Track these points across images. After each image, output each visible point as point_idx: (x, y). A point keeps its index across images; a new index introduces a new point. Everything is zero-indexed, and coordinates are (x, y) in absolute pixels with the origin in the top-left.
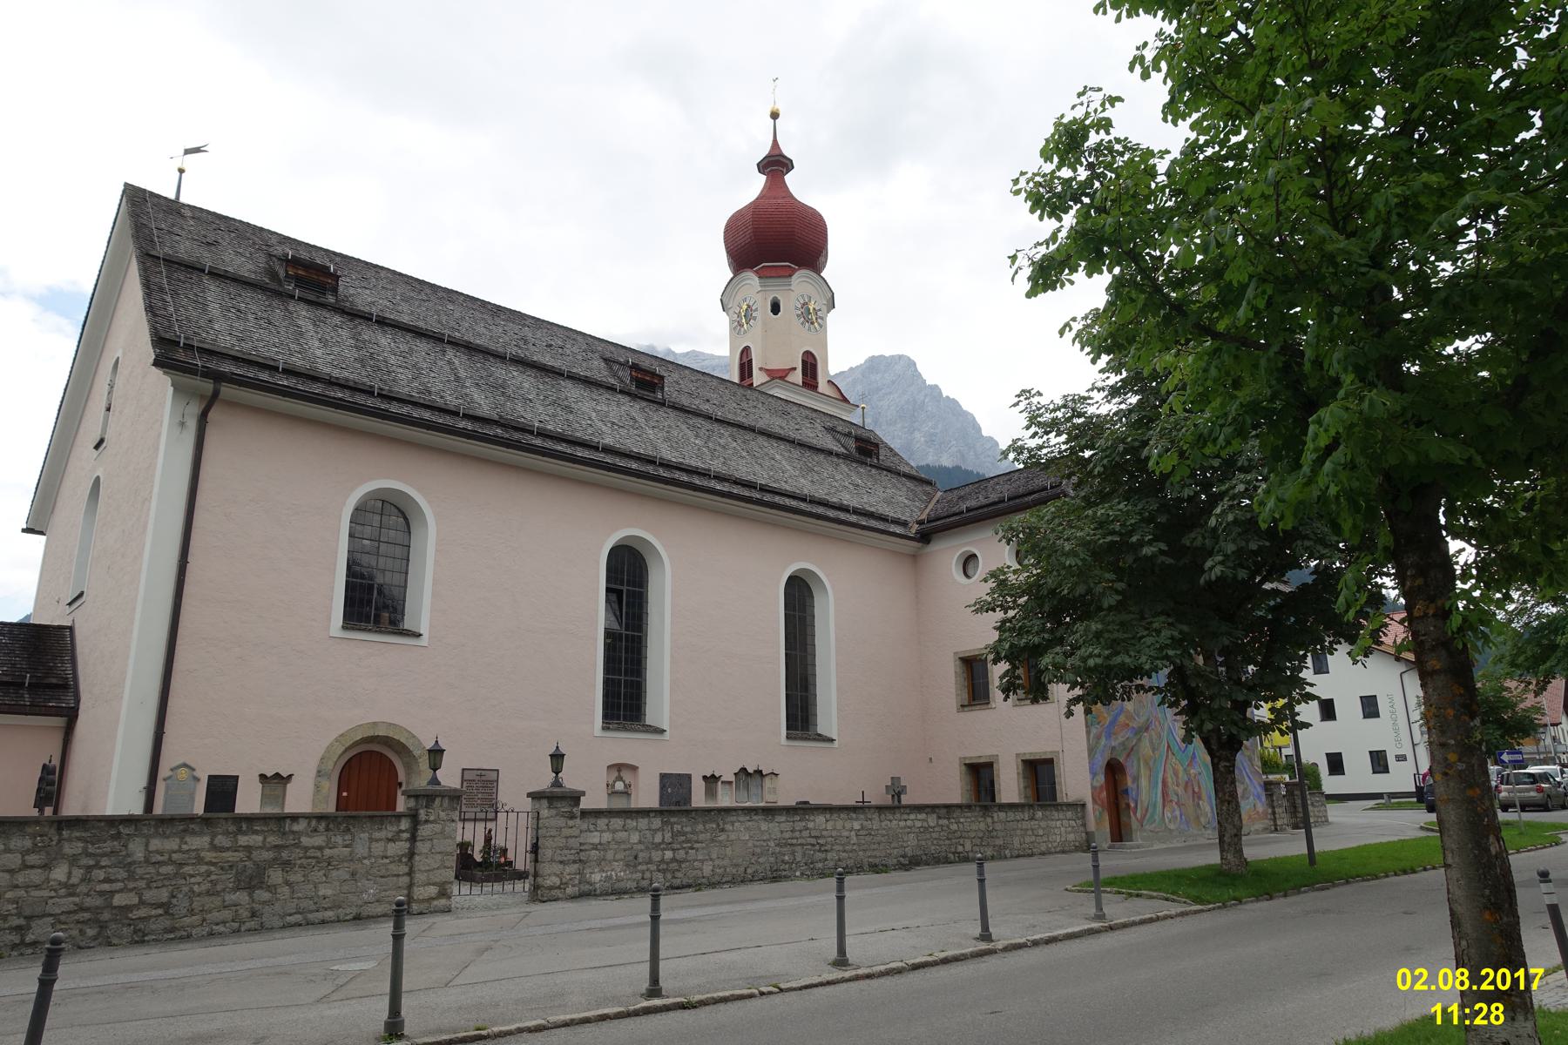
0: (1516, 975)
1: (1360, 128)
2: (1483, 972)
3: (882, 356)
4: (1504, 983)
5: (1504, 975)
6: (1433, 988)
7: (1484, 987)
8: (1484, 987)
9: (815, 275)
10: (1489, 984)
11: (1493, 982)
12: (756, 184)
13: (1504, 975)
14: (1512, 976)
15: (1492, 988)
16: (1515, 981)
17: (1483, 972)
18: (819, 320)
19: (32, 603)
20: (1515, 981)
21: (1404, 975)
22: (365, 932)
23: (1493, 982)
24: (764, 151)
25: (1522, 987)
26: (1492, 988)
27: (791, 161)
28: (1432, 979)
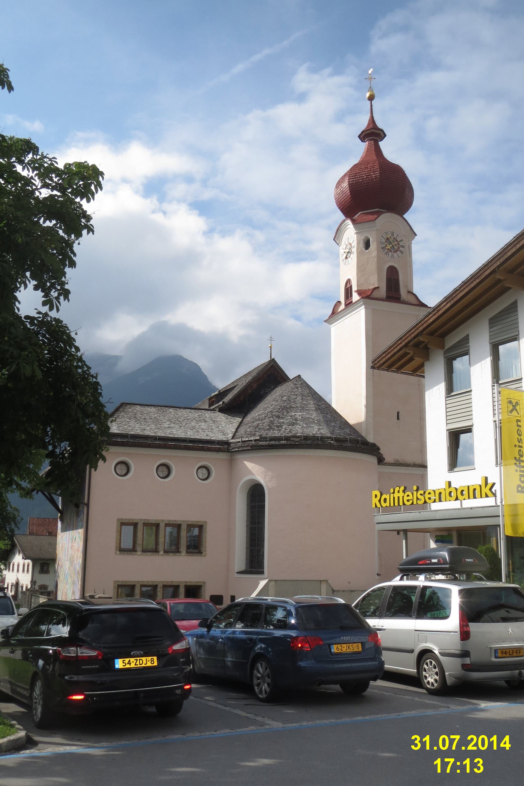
0: (491, 740)
1: (93, 185)
2: (469, 738)
3: (17, 298)
4: (483, 745)
5: (483, 740)
6: (435, 748)
7: (470, 748)
8: (470, 748)
9: (399, 217)
10: (473, 746)
11: (476, 745)
12: (362, 147)
13: (483, 740)
14: (489, 740)
15: (475, 748)
16: (491, 744)
17: (469, 738)
18: (401, 249)
19: (363, 410)
20: (491, 744)
21: (444, 740)
22: (511, 704)
23: (476, 745)
24: (363, 123)
25: (428, 748)
26: (475, 748)
27: (383, 131)
28: (434, 742)
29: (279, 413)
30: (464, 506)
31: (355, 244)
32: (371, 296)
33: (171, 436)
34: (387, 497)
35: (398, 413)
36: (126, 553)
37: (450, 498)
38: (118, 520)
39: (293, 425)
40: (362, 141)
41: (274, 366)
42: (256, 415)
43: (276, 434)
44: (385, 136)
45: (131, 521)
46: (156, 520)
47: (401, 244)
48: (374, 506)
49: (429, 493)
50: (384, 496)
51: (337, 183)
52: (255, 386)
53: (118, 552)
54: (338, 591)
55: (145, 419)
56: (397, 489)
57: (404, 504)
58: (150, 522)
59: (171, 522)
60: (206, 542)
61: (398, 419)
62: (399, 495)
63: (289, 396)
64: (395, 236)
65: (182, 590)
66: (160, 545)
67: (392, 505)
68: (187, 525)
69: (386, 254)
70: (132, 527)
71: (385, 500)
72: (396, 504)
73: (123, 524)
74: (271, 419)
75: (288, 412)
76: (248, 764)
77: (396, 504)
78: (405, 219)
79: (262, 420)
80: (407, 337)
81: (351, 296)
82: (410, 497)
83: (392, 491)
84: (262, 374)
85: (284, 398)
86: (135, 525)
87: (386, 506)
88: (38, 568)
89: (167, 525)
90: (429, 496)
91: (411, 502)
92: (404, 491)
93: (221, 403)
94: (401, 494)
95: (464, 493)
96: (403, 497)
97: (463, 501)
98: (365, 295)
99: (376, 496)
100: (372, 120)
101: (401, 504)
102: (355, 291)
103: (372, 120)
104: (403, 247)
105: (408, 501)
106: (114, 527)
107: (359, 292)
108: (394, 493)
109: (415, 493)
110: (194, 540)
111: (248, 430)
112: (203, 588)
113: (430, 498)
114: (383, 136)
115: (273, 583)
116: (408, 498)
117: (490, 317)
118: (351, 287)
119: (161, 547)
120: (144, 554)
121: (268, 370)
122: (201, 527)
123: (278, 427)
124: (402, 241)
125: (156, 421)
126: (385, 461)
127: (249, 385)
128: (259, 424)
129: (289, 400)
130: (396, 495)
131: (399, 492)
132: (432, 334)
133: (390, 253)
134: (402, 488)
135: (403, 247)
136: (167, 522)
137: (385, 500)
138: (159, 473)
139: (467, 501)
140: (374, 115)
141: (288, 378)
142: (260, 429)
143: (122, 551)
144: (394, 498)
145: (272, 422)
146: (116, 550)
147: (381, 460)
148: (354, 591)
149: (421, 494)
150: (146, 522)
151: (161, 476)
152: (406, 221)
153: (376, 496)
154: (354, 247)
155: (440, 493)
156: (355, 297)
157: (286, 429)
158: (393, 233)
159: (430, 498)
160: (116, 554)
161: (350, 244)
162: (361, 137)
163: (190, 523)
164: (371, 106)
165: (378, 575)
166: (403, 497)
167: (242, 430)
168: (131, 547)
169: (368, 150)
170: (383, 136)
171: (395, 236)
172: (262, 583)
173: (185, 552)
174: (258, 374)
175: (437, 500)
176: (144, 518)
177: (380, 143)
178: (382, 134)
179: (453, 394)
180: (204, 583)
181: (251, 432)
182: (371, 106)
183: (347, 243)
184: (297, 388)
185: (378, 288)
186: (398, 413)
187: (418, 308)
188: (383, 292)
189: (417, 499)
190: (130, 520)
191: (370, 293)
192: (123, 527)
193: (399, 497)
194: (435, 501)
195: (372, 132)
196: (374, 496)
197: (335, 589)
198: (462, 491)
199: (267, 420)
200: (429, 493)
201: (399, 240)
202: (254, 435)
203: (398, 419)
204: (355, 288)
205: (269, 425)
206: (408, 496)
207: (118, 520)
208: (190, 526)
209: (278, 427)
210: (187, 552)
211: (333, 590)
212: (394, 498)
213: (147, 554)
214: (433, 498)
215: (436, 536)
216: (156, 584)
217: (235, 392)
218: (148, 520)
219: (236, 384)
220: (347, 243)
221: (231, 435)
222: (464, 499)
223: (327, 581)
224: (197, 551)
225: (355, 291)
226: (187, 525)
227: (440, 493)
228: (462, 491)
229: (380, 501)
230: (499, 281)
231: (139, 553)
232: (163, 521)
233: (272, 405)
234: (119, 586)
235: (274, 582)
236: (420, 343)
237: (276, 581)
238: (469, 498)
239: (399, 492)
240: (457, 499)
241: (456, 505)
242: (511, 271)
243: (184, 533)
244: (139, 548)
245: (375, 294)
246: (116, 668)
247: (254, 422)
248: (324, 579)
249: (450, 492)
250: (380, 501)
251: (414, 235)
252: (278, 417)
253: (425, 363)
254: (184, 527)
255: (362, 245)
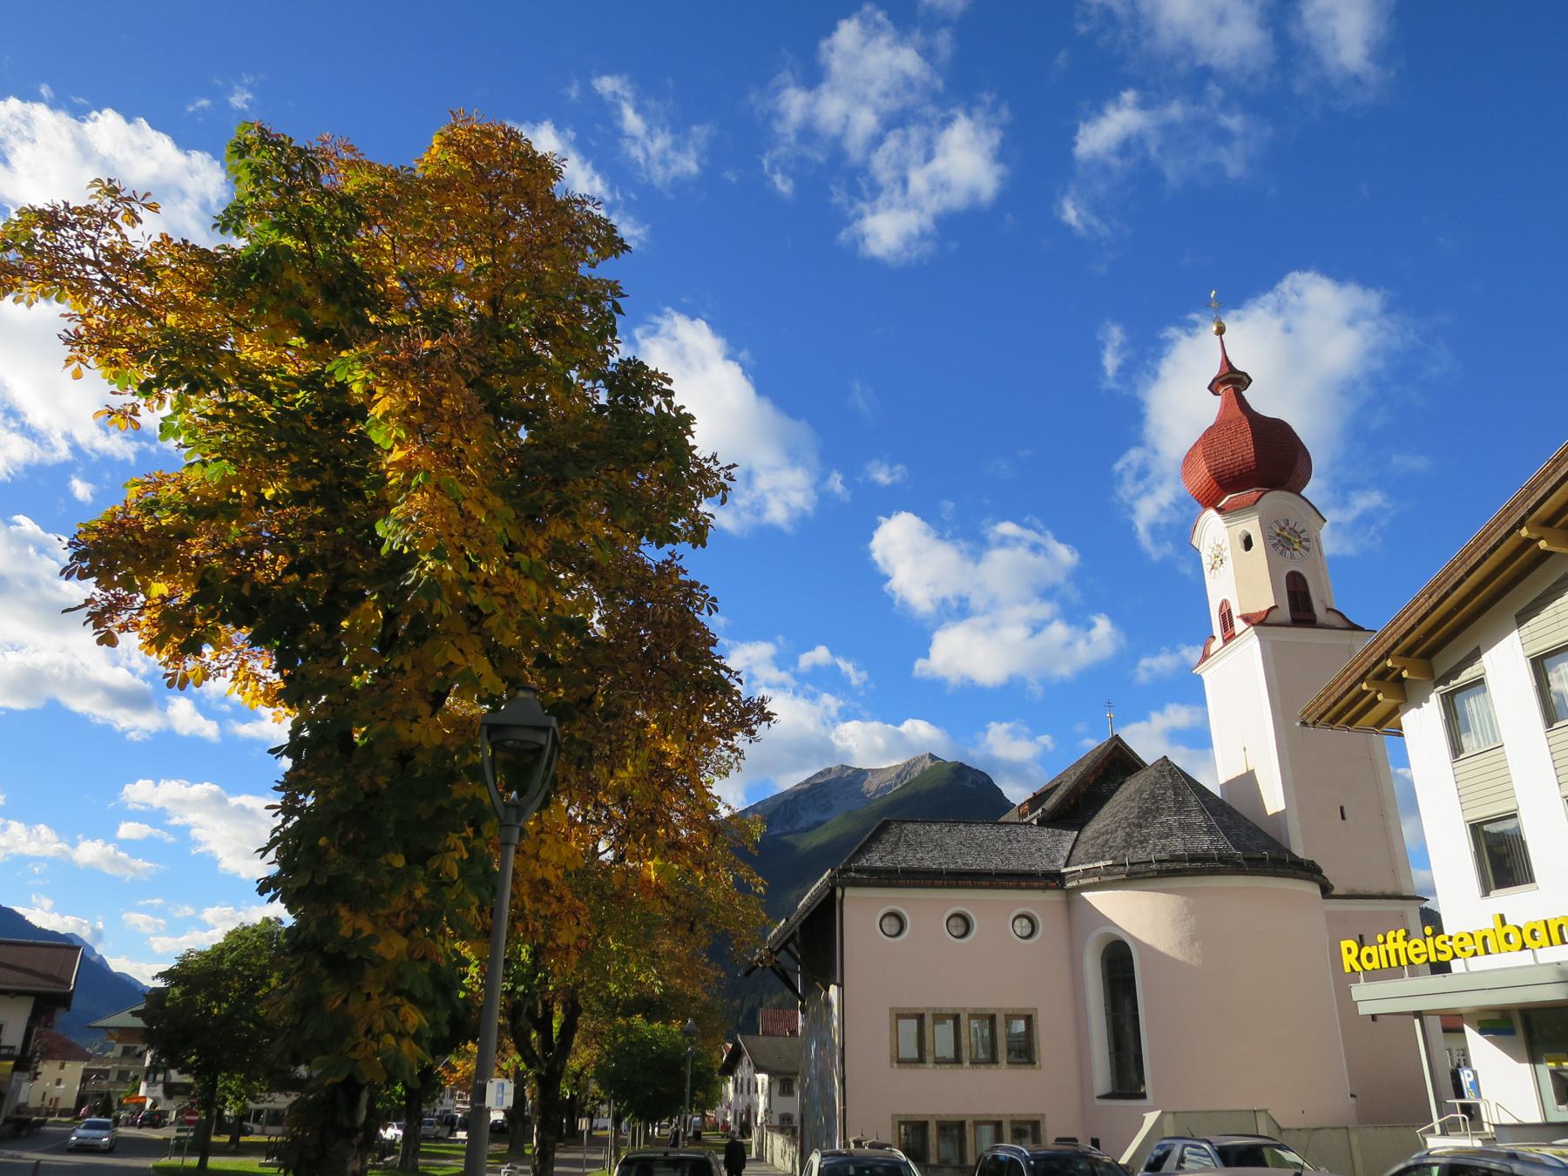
24: (1214, 370)
27: (1246, 374)
29: (1140, 818)
30: (1541, 961)
31: (1227, 545)
32: (1266, 621)
33: (967, 867)
34: (1373, 950)
35: (1342, 808)
36: (909, 1065)
37: (1538, 943)
38: (892, 1009)
39: (1167, 837)
40: (1215, 394)
41: (1120, 749)
42: (1101, 826)
43: (1141, 855)
44: (1250, 381)
45: (913, 1012)
46: (954, 1009)
47: (1303, 536)
48: (1348, 970)
49: (1461, 939)
50: (1365, 951)
51: (1195, 441)
52: (1091, 780)
53: (895, 1065)
54: (1289, 1130)
55: (921, 843)
56: (1391, 935)
57: (1410, 963)
58: (943, 1012)
59: (978, 1012)
60: (1039, 1044)
61: (1343, 818)
62: (1395, 946)
63: (1152, 792)
64: (1291, 525)
65: (1007, 1131)
66: (963, 1051)
67: (1385, 965)
68: (1006, 1015)
69: (1281, 553)
70: (915, 1021)
71: (1369, 957)
72: (1394, 963)
73: (900, 1016)
74: (1127, 830)
75: (1155, 818)
76: (772, 934)
77: (1394, 963)
78: (1303, 498)
79: (1111, 833)
80: (1361, 665)
81: (1232, 625)
82: (1422, 949)
83: (1380, 938)
84: (1101, 760)
85: (1145, 796)
86: (920, 1018)
87: (1374, 969)
88: (777, 1088)
89: (972, 1016)
90: (1461, 944)
91: (1423, 958)
92: (1406, 938)
93: (1040, 811)
94: (1401, 944)
95: (1537, 934)
96: (1406, 949)
97: (1537, 951)
98: (1255, 621)
99: (1349, 951)
100: (1226, 361)
101: (1404, 962)
102: (1238, 617)
103: (1226, 361)
104: (1307, 540)
105: (1417, 956)
106: (885, 1020)
107: (1246, 618)
108: (1385, 942)
109: (1429, 940)
110: (1019, 1041)
111: (1091, 851)
112: (1042, 1125)
113: (1463, 949)
114: (1247, 381)
115: (1169, 1118)
116: (1417, 951)
117: (1517, 611)
118: (1229, 611)
119: (965, 1054)
120: (938, 1067)
121: (1110, 754)
122: (1029, 1020)
123: (1141, 842)
124: (1303, 531)
125: (941, 847)
126: (1334, 892)
127: (1082, 780)
128: (1107, 841)
129: (1154, 797)
130: (1391, 946)
131: (1395, 940)
132: (1408, 653)
133: (1288, 552)
134: (1402, 933)
135: (1307, 540)
136: (972, 1012)
137: (1369, 957)
138: (952, 930)
139: (1548, 950)
140: (1228, 354)
141: (1145, 765)
142: (1111, 847)
143: (901, 1062)
144: (1387, 952)
145: (1129, 835)
146: (891, 1060)
147: (1326, 891)
148: (1317, 1129)
149: (1444, 942)
150: (937, 1012)
151: (955, 934)
152: (1306, 500)
153: (1349, 951)
154: (1226, 549)
155: (1485, 938)
156: (1239, 625)
157: (1155, 845)
158: (1288, 521)
159: (1463, 949)
160: (892, 1067)
161: (1219, 546)
162: (1214, 387)
163: (1010, 1012)
164: (1222, 342)
165: (1352, 1096)
166: (1406, 949)
167: (1079, 852)
168: (916, 1056)
169: (1225, 407)
170: (1247, 381)
171: (1291, 525)
172: (1151, 1118)
173: (1005, 1062)
174: (1094, 762)
175: (1481, 950)
176: (932, 1006)
177: (1244, 393)
178: (1245, 378)
179: (1462, 757)
180: (1043, 1116)
181: (1096, 853)
182: (1222, 342)
183: (1213, 545)
184: (1164, 776)
185: (1276, 607)
186: (1342, 808)
187: (1348, 632)
188: (1285, 613)
189: (1437, 951)
190: (910, 1009)
191: (1264, 616)
192: (900, 1021)
193: (1396, 951)
194: (1475, 954)
195: (1230, 379)
196: (1344, 951)
197: (1283, 1126)
198: (1533, 931)
199: (1121, 834)
200: (1461, 939)
201: (1299, 530)
202: (1103, 858)
203: (1343, 818)
204: (1236, 613)
205: (1125, 841)
206: (1416, 946)
207: (892, 1009)
208: (1010, 1018)
209: (1141, 842)
210: (1008, 1063)
211: (1279, 1127)
212: (1387, 952)
213: (943, 1066)
214: (1470, 949)
215: (1480, 1022)
216: (961, 1119)
217: (1060, 792)
218: (941, 1009)
219: (1059, 782)
220: (1213, 545)
221: (1062, 862)
222: (1541, 947)
223: (1266, 1111)
224: (1025, 1060)
225: (1238, 617)
226: (1006, 1015)
227: (1485, 938)
228: (1533, 931)
229: (1358, 958)
230: (1528, 542)
231: (931, 1066)
232: (964, 1009)
233: (1125, 808)
234: (900, 1123)
235: (1171, 1116)
236: (1387, 671)
237: (1174, 1113)
238: (1551, 944)
239: (1395, 940)
240: (1524, 947)
241: (1526, 958)
242: (1549, 522)
243: (1001, 1031)
244: (929, 1058)
245: (1273, 618)
246: (546, 123)
247: (1098, 837)
248: (1259, 1108)
249: (1507, 936)
250: (1358, 958)
251: (1320, 520)
252: (1140, 826)
253: (1400, 708)
254: (1000, 1020)
255: (1240, 545)
